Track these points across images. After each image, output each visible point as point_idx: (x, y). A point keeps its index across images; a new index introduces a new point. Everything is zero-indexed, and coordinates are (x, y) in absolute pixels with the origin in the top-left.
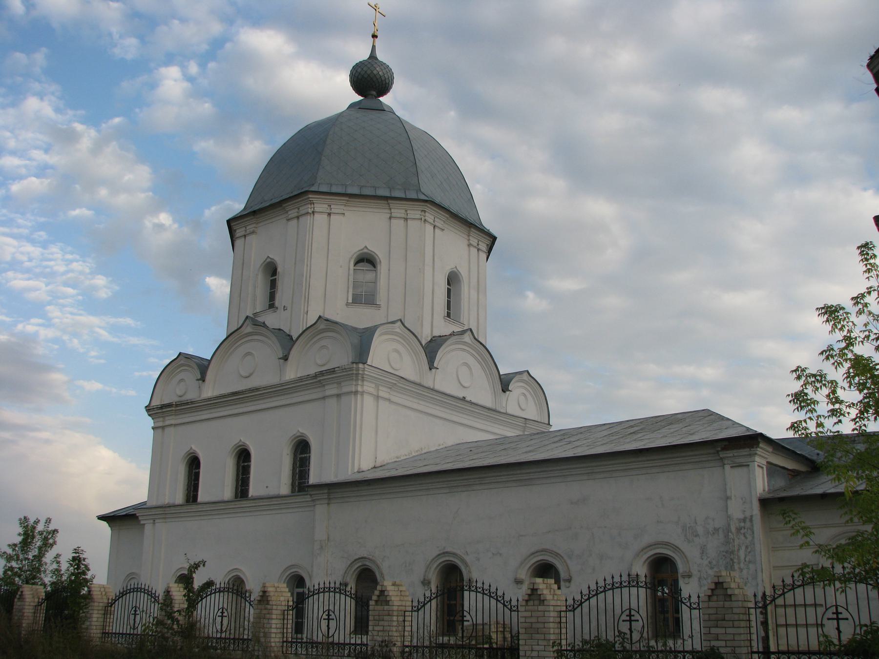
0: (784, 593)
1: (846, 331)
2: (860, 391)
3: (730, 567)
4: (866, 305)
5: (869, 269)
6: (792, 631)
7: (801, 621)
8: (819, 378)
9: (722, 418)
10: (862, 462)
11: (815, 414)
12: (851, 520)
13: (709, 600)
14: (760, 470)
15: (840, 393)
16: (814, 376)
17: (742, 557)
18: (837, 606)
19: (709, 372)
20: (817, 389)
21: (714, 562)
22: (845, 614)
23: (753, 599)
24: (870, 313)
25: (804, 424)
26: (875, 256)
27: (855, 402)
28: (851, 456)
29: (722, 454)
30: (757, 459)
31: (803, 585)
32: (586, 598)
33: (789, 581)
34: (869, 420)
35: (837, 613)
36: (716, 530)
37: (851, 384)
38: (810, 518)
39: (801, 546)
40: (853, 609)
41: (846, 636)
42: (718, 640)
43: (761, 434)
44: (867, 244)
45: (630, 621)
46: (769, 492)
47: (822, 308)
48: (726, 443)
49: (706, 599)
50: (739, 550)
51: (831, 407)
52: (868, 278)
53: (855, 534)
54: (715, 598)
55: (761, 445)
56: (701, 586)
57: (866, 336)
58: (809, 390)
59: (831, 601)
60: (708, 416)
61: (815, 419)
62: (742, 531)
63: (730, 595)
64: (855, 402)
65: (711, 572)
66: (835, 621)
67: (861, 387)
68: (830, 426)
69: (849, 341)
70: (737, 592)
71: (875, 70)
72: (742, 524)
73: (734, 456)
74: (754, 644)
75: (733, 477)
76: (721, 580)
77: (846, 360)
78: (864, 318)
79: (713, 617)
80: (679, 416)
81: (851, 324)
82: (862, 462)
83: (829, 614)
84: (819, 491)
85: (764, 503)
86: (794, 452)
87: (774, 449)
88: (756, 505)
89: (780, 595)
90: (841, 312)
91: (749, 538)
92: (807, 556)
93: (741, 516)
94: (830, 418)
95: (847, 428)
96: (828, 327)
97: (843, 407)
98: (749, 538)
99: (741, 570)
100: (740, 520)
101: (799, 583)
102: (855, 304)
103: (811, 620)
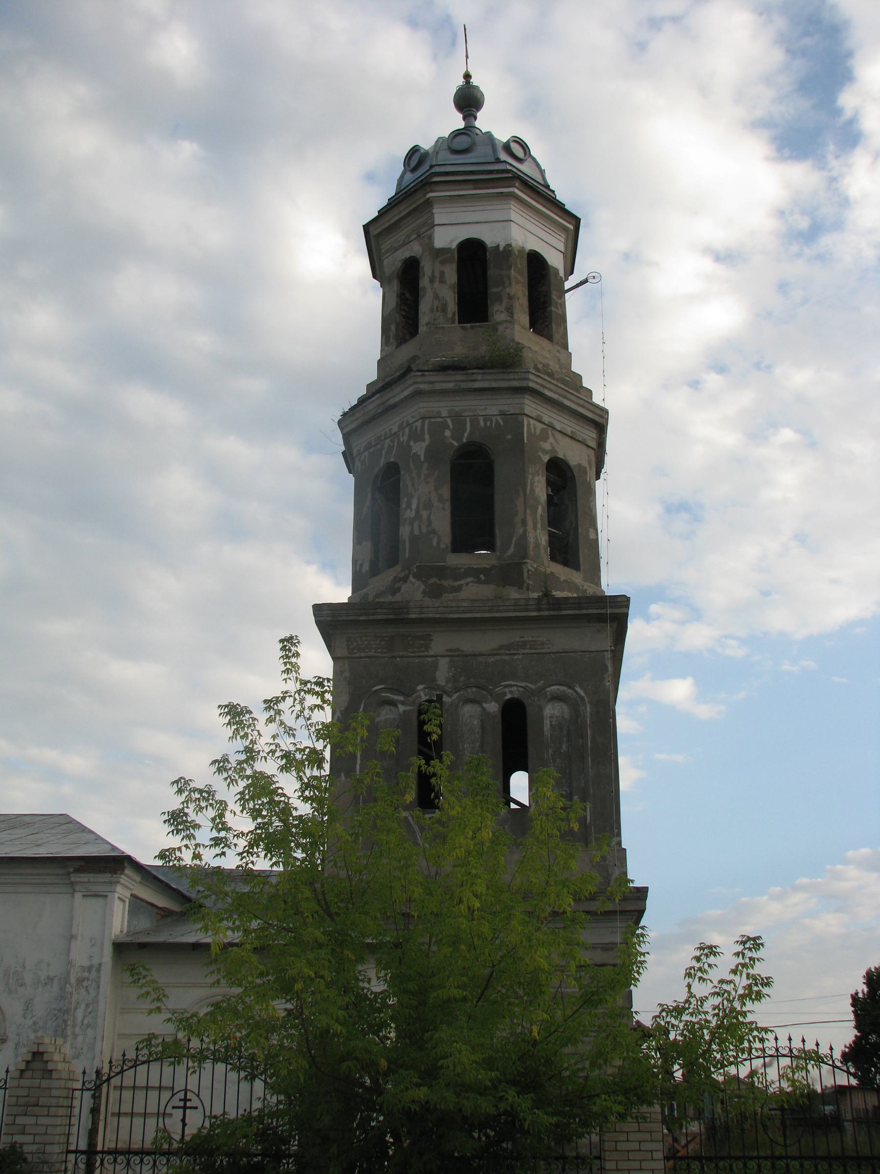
0: (122, 1072)
1: (248, 741)
2: (254, 819)
3: (61, 1032)
4: (279, 712)
5: (288, 669)
6: (138, 1121)
7: (126, 1108)
8: (207, 794)
9: (84, 829)
10: (242, 906)
11: (193, 842)
12: (218, 982)
13: (21, 1077)
14: (121, 904)
15: (228, 817)
16: (201, 791)
17: (79, 1020)
18: (186, 1091)
19: (78, 762)
20: (201, 809)
21: (41, 1024)
22: (195, 1102)
23: (80, 1077)
24: (282, 723)
25: (178, 854)
26: (297, 655)
27: (246, 831)
28: (229, 900)
29: (75, 878)
30: (119, 889)
31: (148, 1062)
32: (131, 1064)
33: (131, 1055)
34: (258, 856)
35: (185, 1100)
36: (50, 979)
37: (244, 809)
38: (160, 973)
39: (150, 1012)
40: (205, 1095)
41: (190, 1131)
42: (23, 1134)
43: (129, 858)
44: (291, 638)
45: (185, 1108)
46: (129, 934)
47: (226, 706)
48: (82, 863)
49: (18, 1074)
50: (76, 1008)
51: (215, 834)
52: (285, 679)
53: (220, 998)
54: (29, 1074)
55: (126, 871)
56: (17, 1056)
57: (271, 751)
58: (190, 810)
59: (180, 1085)
60: (64, 823)
61: (192, 847)
62: (85, 983)
63: (51, 1071)
64: (246, 831)
65: (32, 1036)
66: (181, 1111)
67: (255, 814)
68: (210, 858)
69: (251, 754)
70: (60, 1066)
71: (345, 431)
72: (86, 974)
73: (89, 882)
74: (73, 1139)
75: (84, 909)
76: (41, 1050)
77: (242, 778)
78: (273, 727)
79: (22, 1101)
80: (27, 819)
81: (256, 733)
82: (242, 906)
83: (176, 1102)
84: (191, 939)
85: (120, 948)
86: (168, 886)
87: (142, 878)
88: (108, 950)
89: (118, 1074)
90: (247, 716)
91: (93, 993)
92: (160, 1025)
93: (86, 963)
94: (213, 849)
95: (231, 862)
96: (229, 731)
97: (230, 836)
98: (93, 993)
99: (75, 1036)
100: (83, 968)
101: (145, 1059)
102: (266, 709)
103: (152, 1108)
